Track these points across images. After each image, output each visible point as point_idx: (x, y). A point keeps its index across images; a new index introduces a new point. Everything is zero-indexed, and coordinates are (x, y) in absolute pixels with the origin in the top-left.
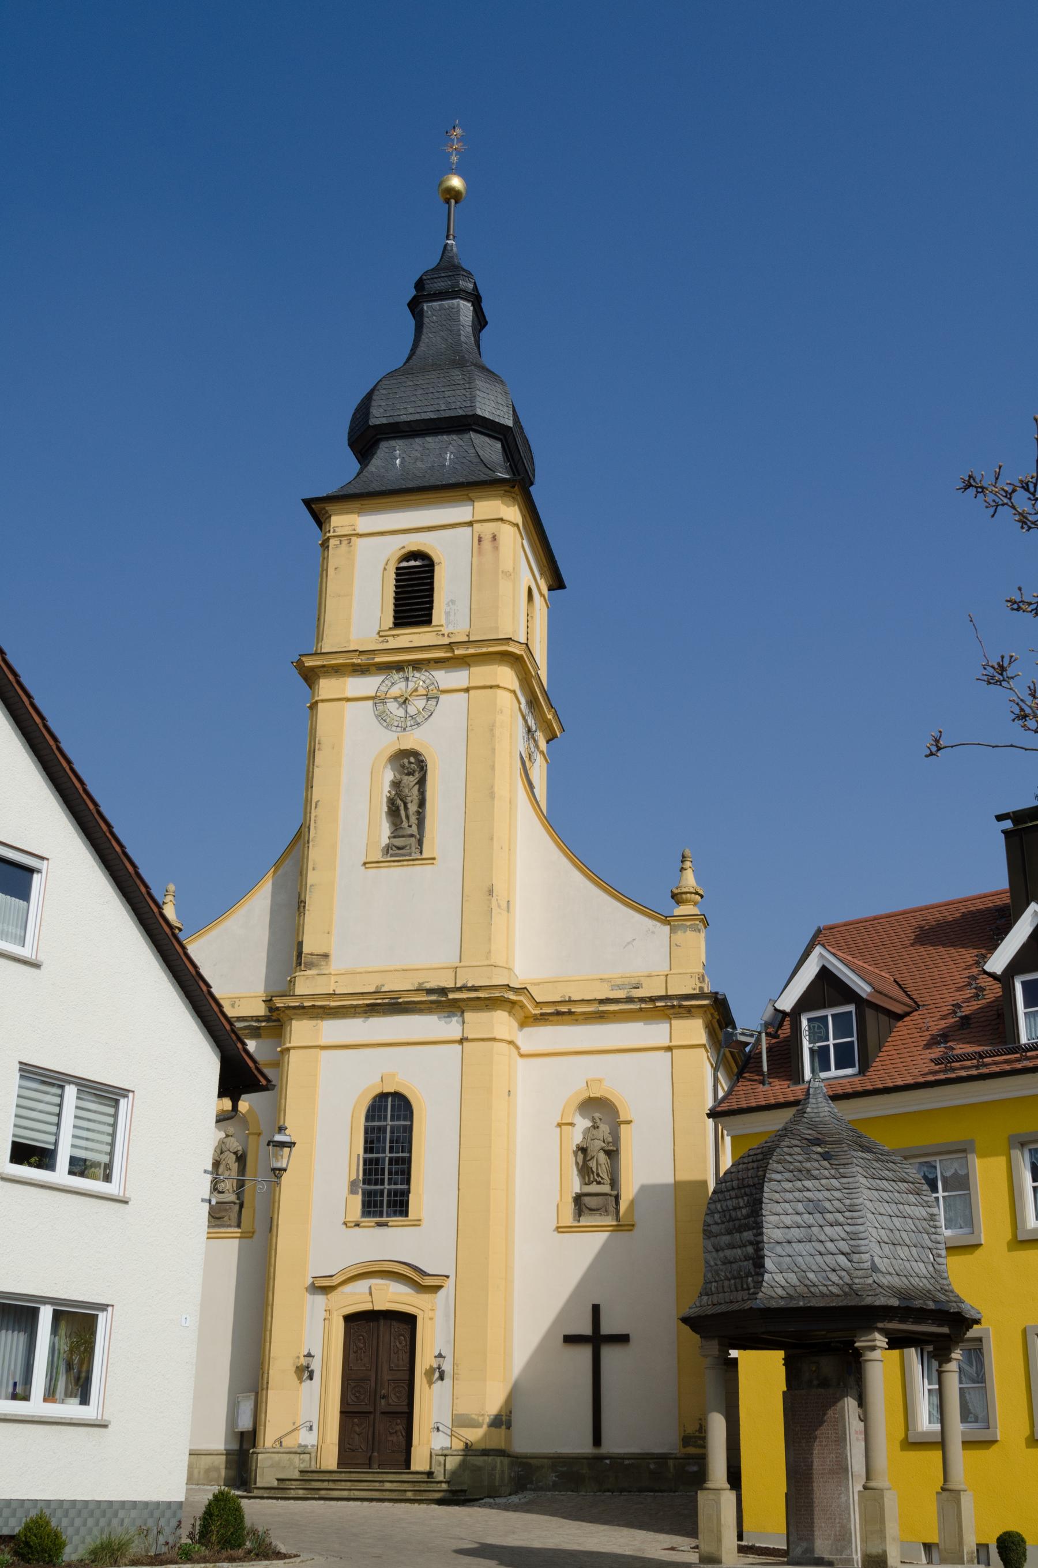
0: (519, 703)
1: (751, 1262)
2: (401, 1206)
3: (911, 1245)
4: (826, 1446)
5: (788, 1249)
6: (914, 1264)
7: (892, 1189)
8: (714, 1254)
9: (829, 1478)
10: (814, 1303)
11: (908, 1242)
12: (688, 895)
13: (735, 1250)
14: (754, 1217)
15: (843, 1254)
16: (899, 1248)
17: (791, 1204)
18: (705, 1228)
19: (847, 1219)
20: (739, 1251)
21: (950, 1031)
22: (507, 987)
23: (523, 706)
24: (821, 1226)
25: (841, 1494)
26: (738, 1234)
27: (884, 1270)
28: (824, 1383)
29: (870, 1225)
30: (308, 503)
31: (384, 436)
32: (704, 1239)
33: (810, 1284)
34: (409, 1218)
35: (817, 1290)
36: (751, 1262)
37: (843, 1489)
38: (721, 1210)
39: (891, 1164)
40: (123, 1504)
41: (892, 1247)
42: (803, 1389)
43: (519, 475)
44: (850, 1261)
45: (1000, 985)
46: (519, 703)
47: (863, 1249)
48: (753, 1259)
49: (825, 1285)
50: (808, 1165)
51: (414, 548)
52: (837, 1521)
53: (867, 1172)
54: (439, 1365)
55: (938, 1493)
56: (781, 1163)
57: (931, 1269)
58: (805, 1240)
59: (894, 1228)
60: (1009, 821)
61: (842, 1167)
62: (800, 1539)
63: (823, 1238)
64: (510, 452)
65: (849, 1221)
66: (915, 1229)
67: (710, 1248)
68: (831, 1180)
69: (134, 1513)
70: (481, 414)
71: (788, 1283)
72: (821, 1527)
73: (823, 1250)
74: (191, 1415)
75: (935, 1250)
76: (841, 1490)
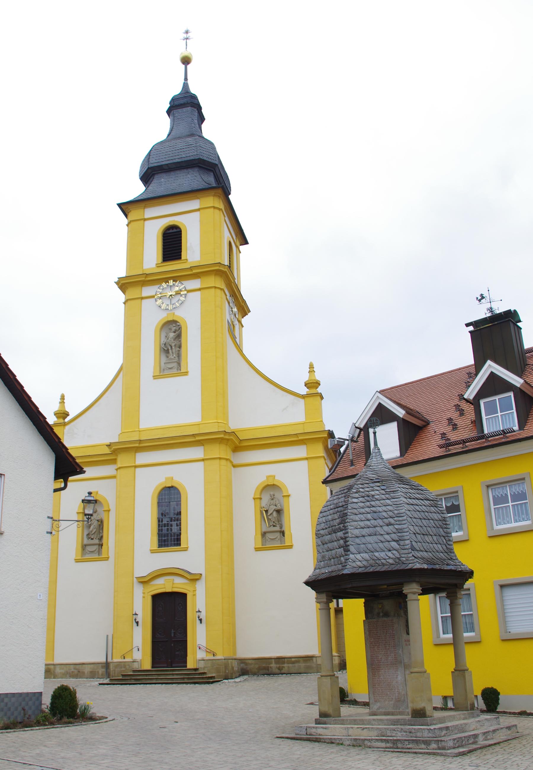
0: (226, 295)
1: (342, 548)
2: (177, 541)
3: (433, 534)
4: (388, 649)
5: (363, 540)
6: (435, 545)
7: (421, 504)
8: (322, 546)
9: (391, 667)
10: (378, 569)
11: (431, 533)
12: (310, 384)
13: (333, 543)
14: (343, 524)
15: (394, 541)
16: (426, 536)
17: (364, 515)
18: (317, 532)
19: (396, 521)
20: (335, 543)
21: (446, 432)
22: (224, 432)
23: (228, 297)
24: (381, 526)
25: (397, 676)
26: (334, 534)
27: (418, 549)
28: (386, 615)
29: (409, 524)
30: (120, 205)
31: (155, 172)
32: (316, 538)
33: (376, 558)
34: (182, 546)
35: (381, 562)
36: (342, 548)
37: (399, 673)
38: (325, 522)
39: (420, 491)
40: (7, 695)
41: (422, 536)
42: (374, 618)
43: (221, 184)
44: (399, 545)
45: (473, 406)
46: (226, 295)
47: (406, 538)
48: (342, 547)
49: (385, 559)
50: (373, 493)
51: (171, 224)
52: (396, 690)
53: (406, 495)
54: (199, 616)
55: (452, 672)
56: (357, 493)
57: (444, 547)
58: (372, 534)
59: (423, 525)
60: (472, 326)
61: (392, 493)
62: (376, 701)
63: (382, 533)
64: (218, 177)
65: (397, 522)
66: (435, 526)
67: (320, 543)
68: (386, 500)
69: (13, 700)
70: (202, 158)
71: (363, 559)
72: (387, 694)
73: (383, 540)
74: (45, 646)
75: (446, 537)
76: (398, 673)
